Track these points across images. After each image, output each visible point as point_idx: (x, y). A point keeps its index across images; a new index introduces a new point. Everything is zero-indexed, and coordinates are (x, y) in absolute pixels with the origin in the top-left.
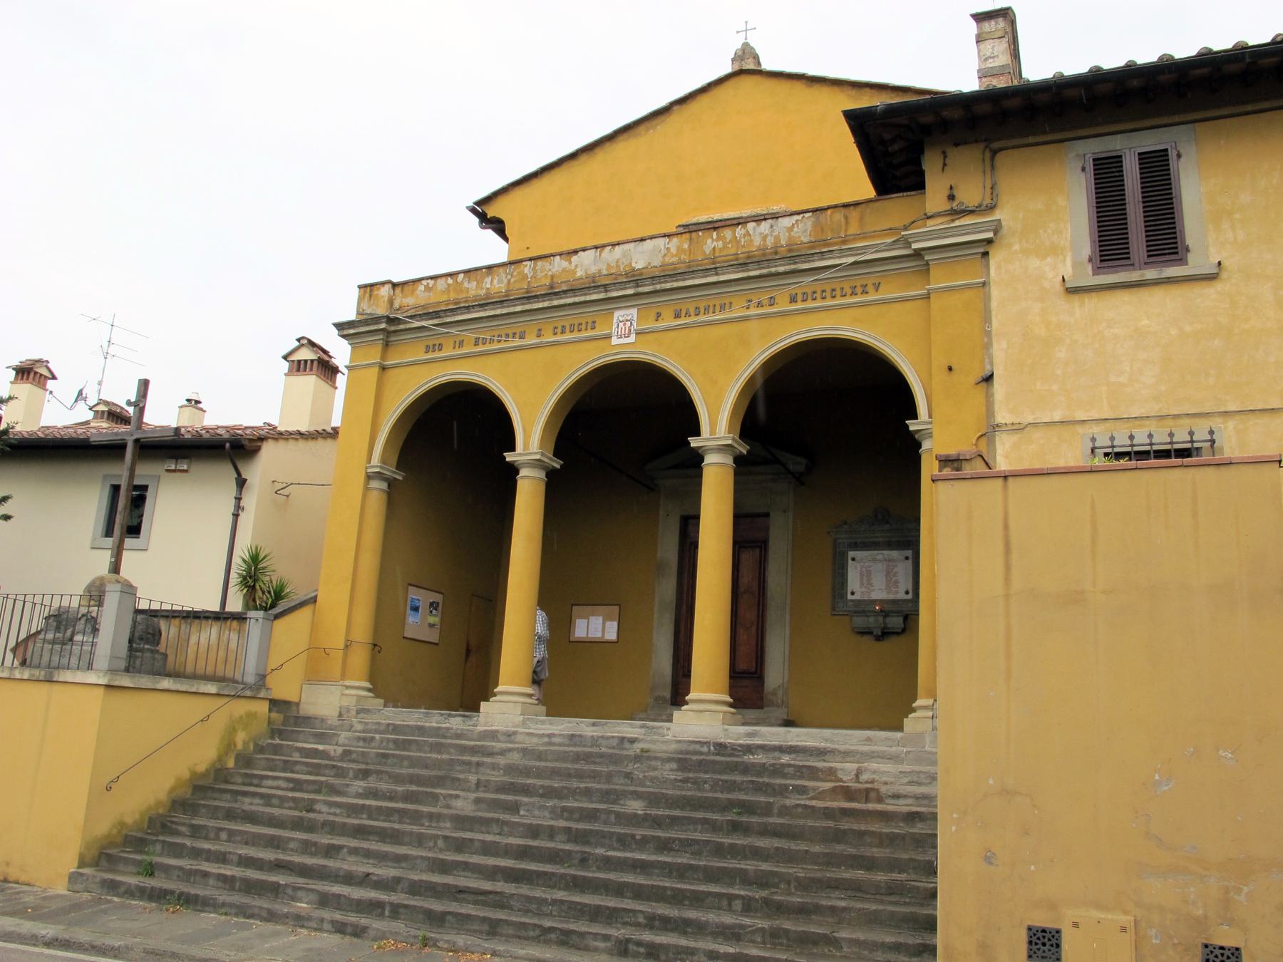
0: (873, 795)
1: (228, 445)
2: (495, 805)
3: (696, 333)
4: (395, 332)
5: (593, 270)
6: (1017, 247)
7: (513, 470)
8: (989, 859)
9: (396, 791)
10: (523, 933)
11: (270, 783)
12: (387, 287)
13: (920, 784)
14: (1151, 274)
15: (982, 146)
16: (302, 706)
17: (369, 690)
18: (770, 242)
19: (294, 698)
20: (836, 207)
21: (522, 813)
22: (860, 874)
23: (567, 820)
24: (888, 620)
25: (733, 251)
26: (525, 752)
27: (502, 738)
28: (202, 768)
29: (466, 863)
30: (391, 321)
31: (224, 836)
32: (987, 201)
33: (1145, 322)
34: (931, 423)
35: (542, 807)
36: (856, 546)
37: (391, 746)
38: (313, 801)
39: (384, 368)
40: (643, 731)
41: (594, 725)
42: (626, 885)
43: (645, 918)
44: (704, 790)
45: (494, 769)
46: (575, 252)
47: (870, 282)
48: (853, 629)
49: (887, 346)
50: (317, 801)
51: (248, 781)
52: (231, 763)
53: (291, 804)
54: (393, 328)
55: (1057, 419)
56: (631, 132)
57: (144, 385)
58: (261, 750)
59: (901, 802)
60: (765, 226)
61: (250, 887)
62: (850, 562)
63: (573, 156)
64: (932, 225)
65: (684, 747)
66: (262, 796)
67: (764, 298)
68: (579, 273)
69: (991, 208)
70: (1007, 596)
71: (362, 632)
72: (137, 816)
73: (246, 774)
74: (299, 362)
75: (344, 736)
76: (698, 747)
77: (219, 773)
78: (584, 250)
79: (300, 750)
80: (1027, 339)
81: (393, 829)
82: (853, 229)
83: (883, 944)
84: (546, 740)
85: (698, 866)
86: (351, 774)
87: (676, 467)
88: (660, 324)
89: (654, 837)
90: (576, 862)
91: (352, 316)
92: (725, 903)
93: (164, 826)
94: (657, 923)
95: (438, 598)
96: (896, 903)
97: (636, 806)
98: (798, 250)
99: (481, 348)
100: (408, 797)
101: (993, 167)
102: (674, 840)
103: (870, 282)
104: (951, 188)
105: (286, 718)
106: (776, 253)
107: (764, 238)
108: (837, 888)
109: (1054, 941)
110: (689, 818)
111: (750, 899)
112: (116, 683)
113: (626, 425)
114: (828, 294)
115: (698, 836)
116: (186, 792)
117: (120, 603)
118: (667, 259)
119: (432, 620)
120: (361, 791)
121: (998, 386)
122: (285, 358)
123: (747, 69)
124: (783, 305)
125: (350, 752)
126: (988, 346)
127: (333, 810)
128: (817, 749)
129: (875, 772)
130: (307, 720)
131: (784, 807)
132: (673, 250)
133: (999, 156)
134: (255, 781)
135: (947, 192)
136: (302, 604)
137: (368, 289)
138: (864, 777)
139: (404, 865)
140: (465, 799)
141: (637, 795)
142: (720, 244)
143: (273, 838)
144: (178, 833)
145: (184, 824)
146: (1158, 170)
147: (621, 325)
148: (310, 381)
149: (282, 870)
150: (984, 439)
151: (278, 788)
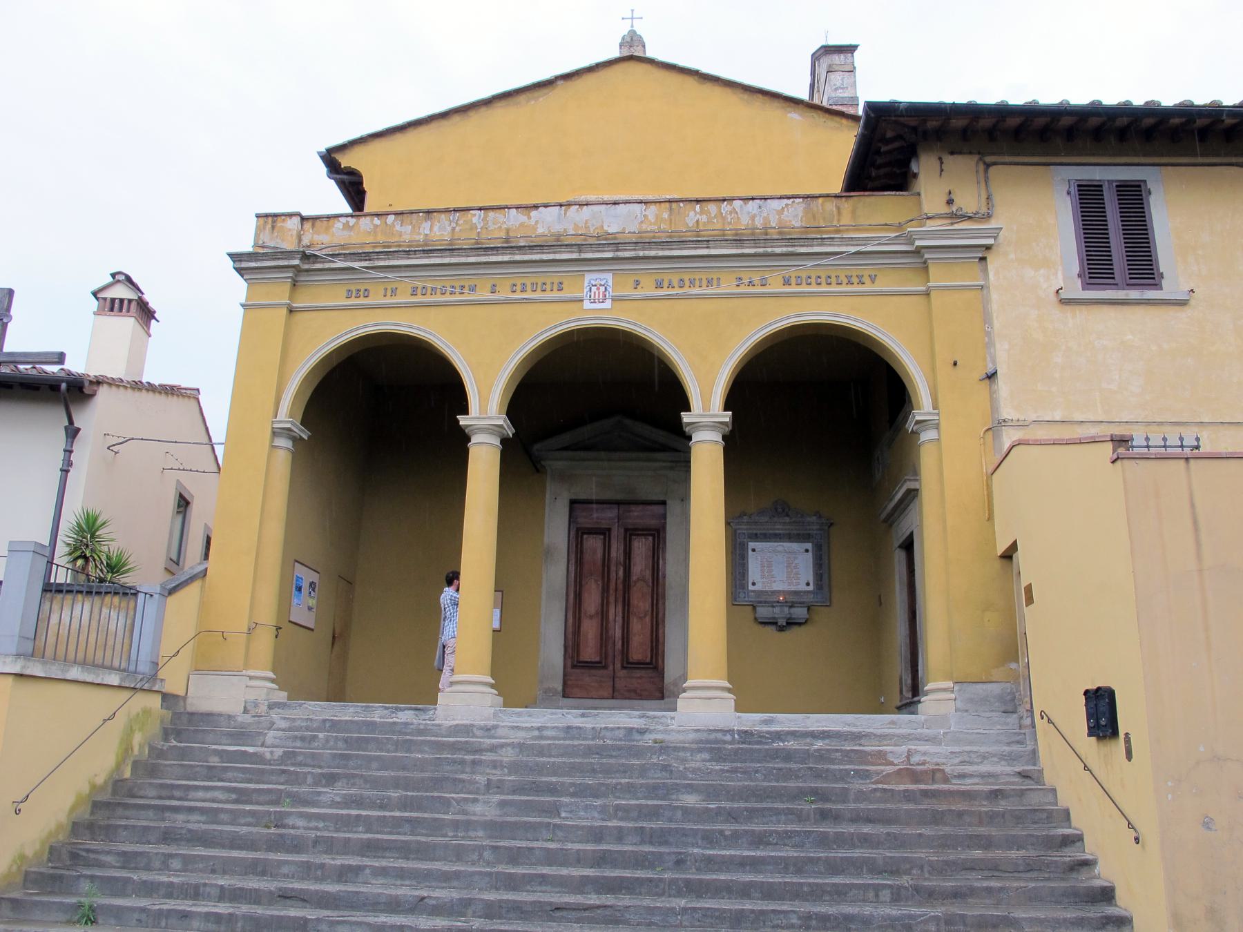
0: (938, 775)
1: (64, 386)
2: (528, 807)
3: (681, 306)
4: (307, 270)
5: (558, 228)
6: (1012, 256)
8: (1207, 824)
9: (389, 798)
11: (200, 794)
12: (296, 220)
13: (971, 763)
14: (1134, 294)
15: (976, 157)
16: (189, 701)
18: (759, 223)
19: (181, 693)
20: (828, 196)
21: (563, 815)
22: (978, 854)
23: (621, 819)
24: (793, 610)
25: (719, 227)
26: (521, 747)
27: (478, 733)
28: (100, 780)
29: (543, 876)
30: (306, 257)
31: (176, 864)
32: (984, 210)
33: (1130, 337)
35: (587, 808)
36: (755, 537)
37: (340, 744)
38: (283, 815)
39: (291, 311)
40: (642, 721)
41: (583, 716)
42: (752, 884)
43: (799, 918)
44: (756, 780)
45: (495, 767)
46: (536, 207)
47: (866, 274)
48: (756, 619)
49: (888, 336)
50: (290, 814)
51: (164, 793)
52: (127, 773)
53: (250, 820)
54: (306, 267)
55: (1058, 419)
56: (511, 100)
58: (161, 754)
59: (968, 781)
60: (752, 205)
62: (750, 552)
63: (444, 115)
64: (930, 225)
65: (704, 736)
66: (202, 811)
67: (756, 278)
68: (540, 230)
69: (988, 217)
70: (1200, 571)
72: (38, 846)
73: (162, 786)
74: (113, 300)
75: (271, 736)
76: (719, 736)
77: (117, 784)
78: (546, 206)
79: (216, 752)
80: (1005, 340)
81: (418, 842)
82: (846, 220)
83: (1065, 920)
84: (536, 733)
85: (819, 858)
86: (309, 780)
87: (566, 449)
88: (639, 293)
89: (746, 832)
90: (670, 864)
91: (247, 247)
92: (871, 894)
93: (74, 856)
94: (814, 923)
95: (315, 577)
96: (1036, 879)
97: (691, 800)
98: (789, 233)
99: (419, 299)
100: (404, 805)
101: (986, 181)
102: (771, 833)
103: (866, 274)
105: (174, 714)
106: (766, 234)
107: (753, 218)
108: (973, 869)
110: (770, 809)
111: (900, 888)
112: (28, 672)
113: (597, 401)
114: (823, 280)
116: (85, 814)
117: (32, 568)
118: (644, 227)
119: (312, 602)
120: (338, 799)
121: (1001, 382)
122: (95, 294)
123: (632, 56)
124: (776, 286)
125: (294, 754)
126: (990, 345)
127: (313, 824)
128: (852, 733)
129: (925, 754)
130: (208, 717)
131: (861, 792)
132: (651, 218)
133: (992, 170)
134: (177, 793)
135: (945, 198)
136: (192, 579)
137: (270, 219)
138: (914, 759)
139: (455, 883)
140: (486, 802)
141: (691, 789)
142: (704, 218)
143: (255, 862)
144: (101, 865)
145: (109, 853)
146: (1133, 199)
147: (594, 289)
148: (127, 324)
149: (289, 902)
150: (990, 433)
151: (214, 801)
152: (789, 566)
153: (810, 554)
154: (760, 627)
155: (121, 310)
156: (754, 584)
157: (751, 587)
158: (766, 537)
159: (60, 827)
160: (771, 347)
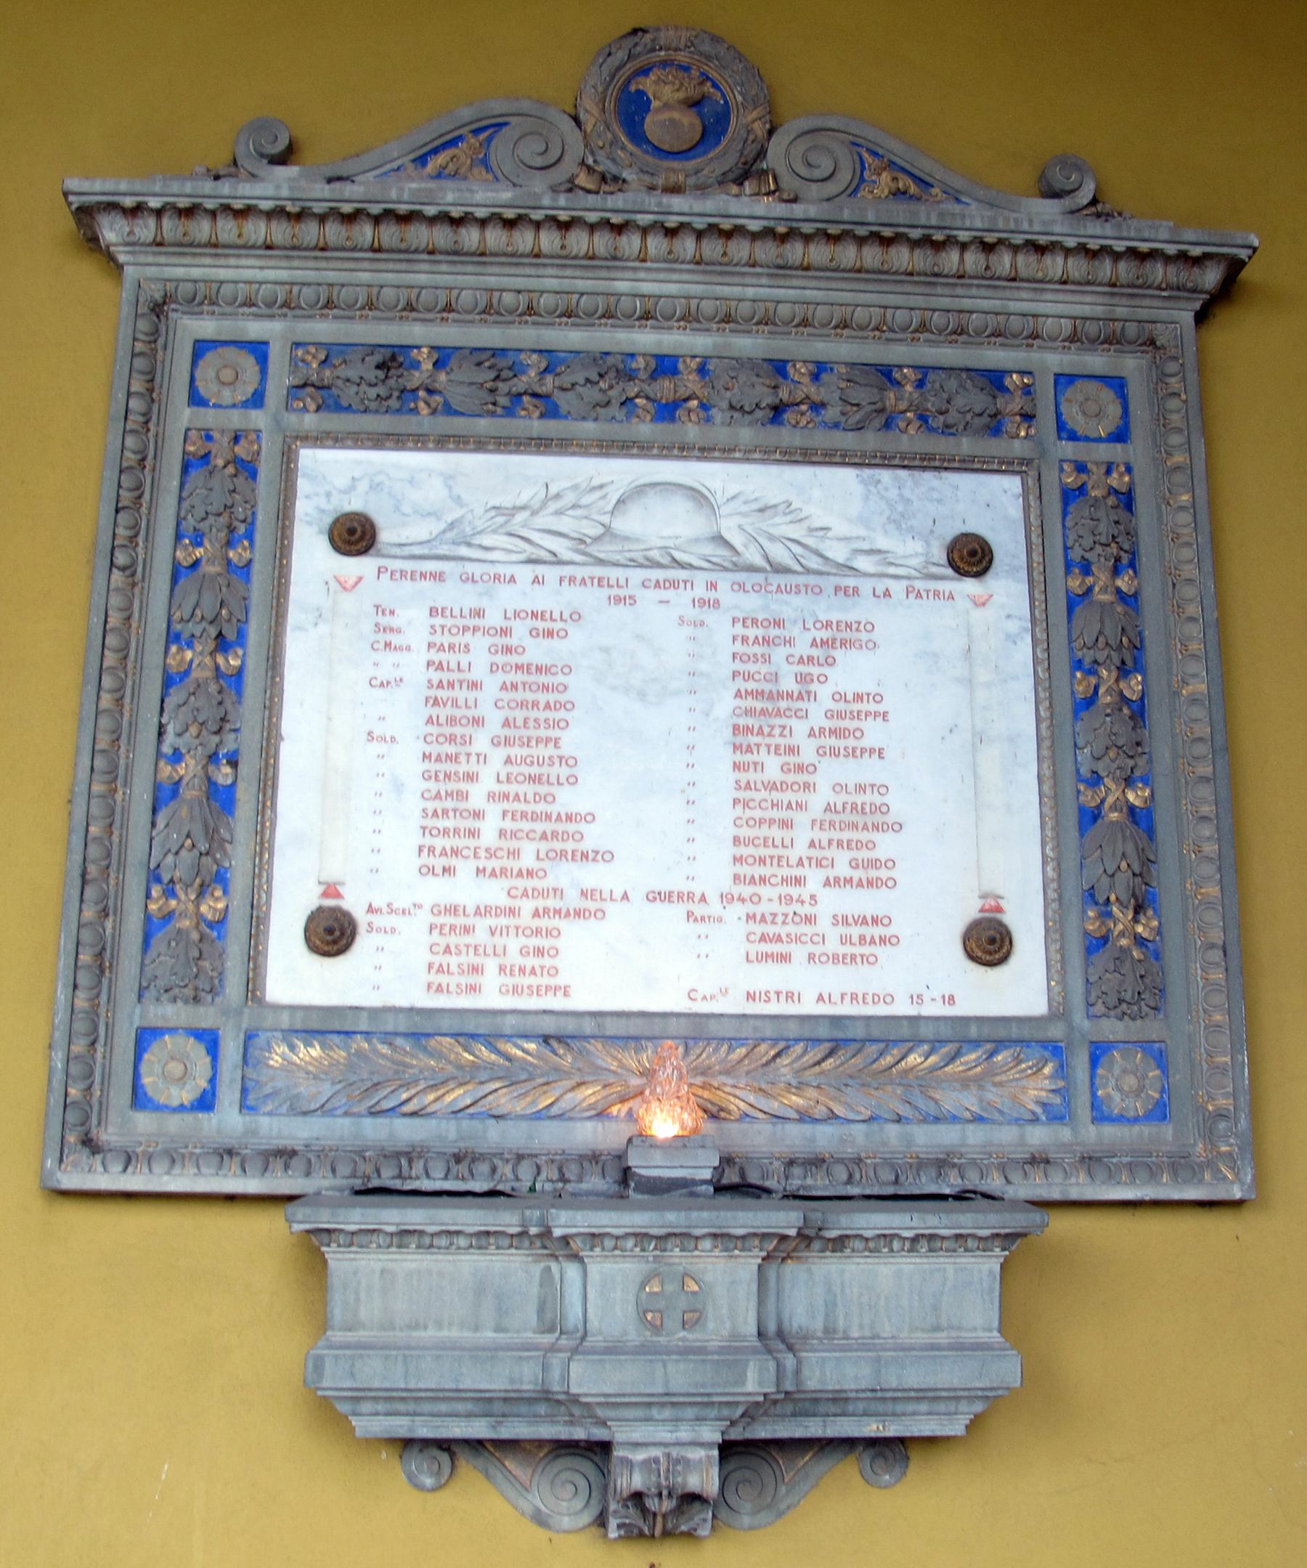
24: (811, 1288)
36: (389, 392)
57: (360, 579)
62: (312, 556)
152: (762, 712)
153: (1002, 605)
154: (397, 1497)
157: (294, 976)
158: (512, 399)
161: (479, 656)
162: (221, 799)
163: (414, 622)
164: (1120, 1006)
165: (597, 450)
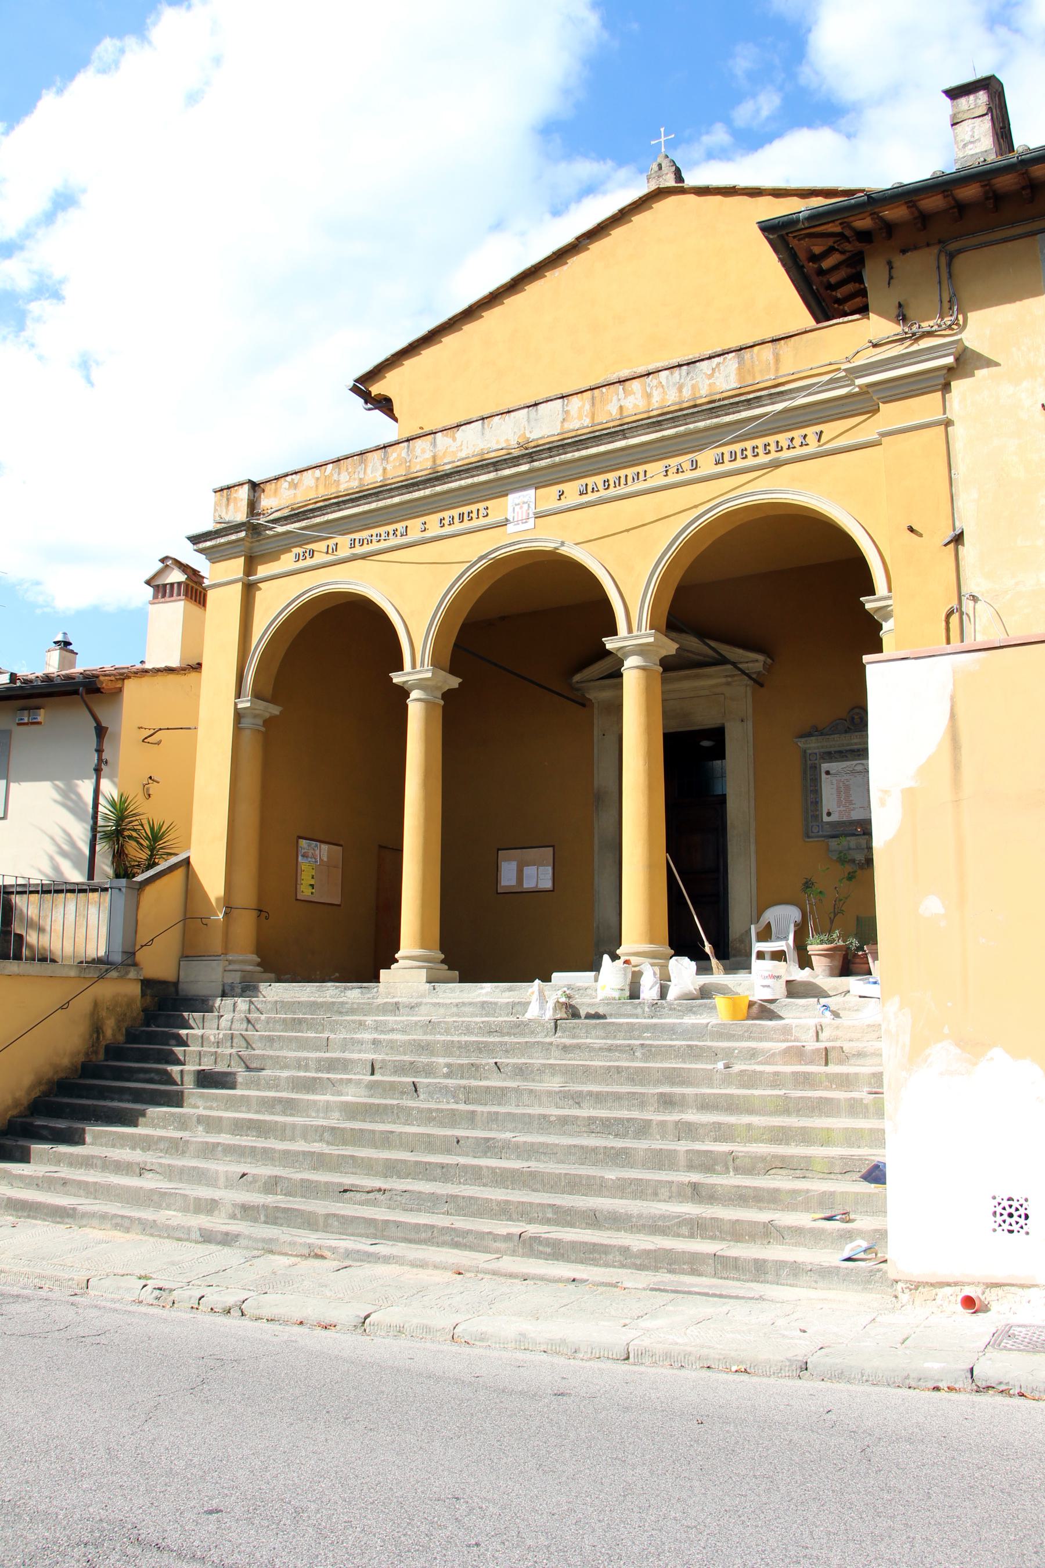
7: (402, 693)
9: (278, 1078)
10: (413, 1235)
15: (935, 250)
16: (181, 986)
17: (259, 965)
18: (687, 393)
34: (889, 598)
43: (556, 1213)
61: (275, 1216)
62: (824, 776)
63: (806, 332)
70: (957, 802)
71: (246, 896)
88: (565, 503)
91: (210, 526)
101: (950, 275)
104: (900, 305)
109: (1022, 1211)
113: (531, 632)
115: (624, 1114)
133: (960, 261)
147: (517, 508)
148: (177, 608)
155: (172, 595)
156: (829, 814)
157: (826, 819)
159: (16, 1103)
160: (720, 541)
161: (841, 784)
162: (817, 803)
163: (835, 782)
164: (107, 1048)
165: (889, 214)
